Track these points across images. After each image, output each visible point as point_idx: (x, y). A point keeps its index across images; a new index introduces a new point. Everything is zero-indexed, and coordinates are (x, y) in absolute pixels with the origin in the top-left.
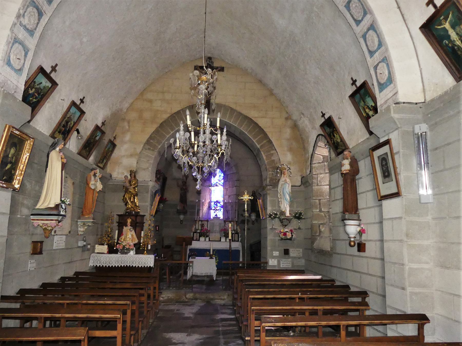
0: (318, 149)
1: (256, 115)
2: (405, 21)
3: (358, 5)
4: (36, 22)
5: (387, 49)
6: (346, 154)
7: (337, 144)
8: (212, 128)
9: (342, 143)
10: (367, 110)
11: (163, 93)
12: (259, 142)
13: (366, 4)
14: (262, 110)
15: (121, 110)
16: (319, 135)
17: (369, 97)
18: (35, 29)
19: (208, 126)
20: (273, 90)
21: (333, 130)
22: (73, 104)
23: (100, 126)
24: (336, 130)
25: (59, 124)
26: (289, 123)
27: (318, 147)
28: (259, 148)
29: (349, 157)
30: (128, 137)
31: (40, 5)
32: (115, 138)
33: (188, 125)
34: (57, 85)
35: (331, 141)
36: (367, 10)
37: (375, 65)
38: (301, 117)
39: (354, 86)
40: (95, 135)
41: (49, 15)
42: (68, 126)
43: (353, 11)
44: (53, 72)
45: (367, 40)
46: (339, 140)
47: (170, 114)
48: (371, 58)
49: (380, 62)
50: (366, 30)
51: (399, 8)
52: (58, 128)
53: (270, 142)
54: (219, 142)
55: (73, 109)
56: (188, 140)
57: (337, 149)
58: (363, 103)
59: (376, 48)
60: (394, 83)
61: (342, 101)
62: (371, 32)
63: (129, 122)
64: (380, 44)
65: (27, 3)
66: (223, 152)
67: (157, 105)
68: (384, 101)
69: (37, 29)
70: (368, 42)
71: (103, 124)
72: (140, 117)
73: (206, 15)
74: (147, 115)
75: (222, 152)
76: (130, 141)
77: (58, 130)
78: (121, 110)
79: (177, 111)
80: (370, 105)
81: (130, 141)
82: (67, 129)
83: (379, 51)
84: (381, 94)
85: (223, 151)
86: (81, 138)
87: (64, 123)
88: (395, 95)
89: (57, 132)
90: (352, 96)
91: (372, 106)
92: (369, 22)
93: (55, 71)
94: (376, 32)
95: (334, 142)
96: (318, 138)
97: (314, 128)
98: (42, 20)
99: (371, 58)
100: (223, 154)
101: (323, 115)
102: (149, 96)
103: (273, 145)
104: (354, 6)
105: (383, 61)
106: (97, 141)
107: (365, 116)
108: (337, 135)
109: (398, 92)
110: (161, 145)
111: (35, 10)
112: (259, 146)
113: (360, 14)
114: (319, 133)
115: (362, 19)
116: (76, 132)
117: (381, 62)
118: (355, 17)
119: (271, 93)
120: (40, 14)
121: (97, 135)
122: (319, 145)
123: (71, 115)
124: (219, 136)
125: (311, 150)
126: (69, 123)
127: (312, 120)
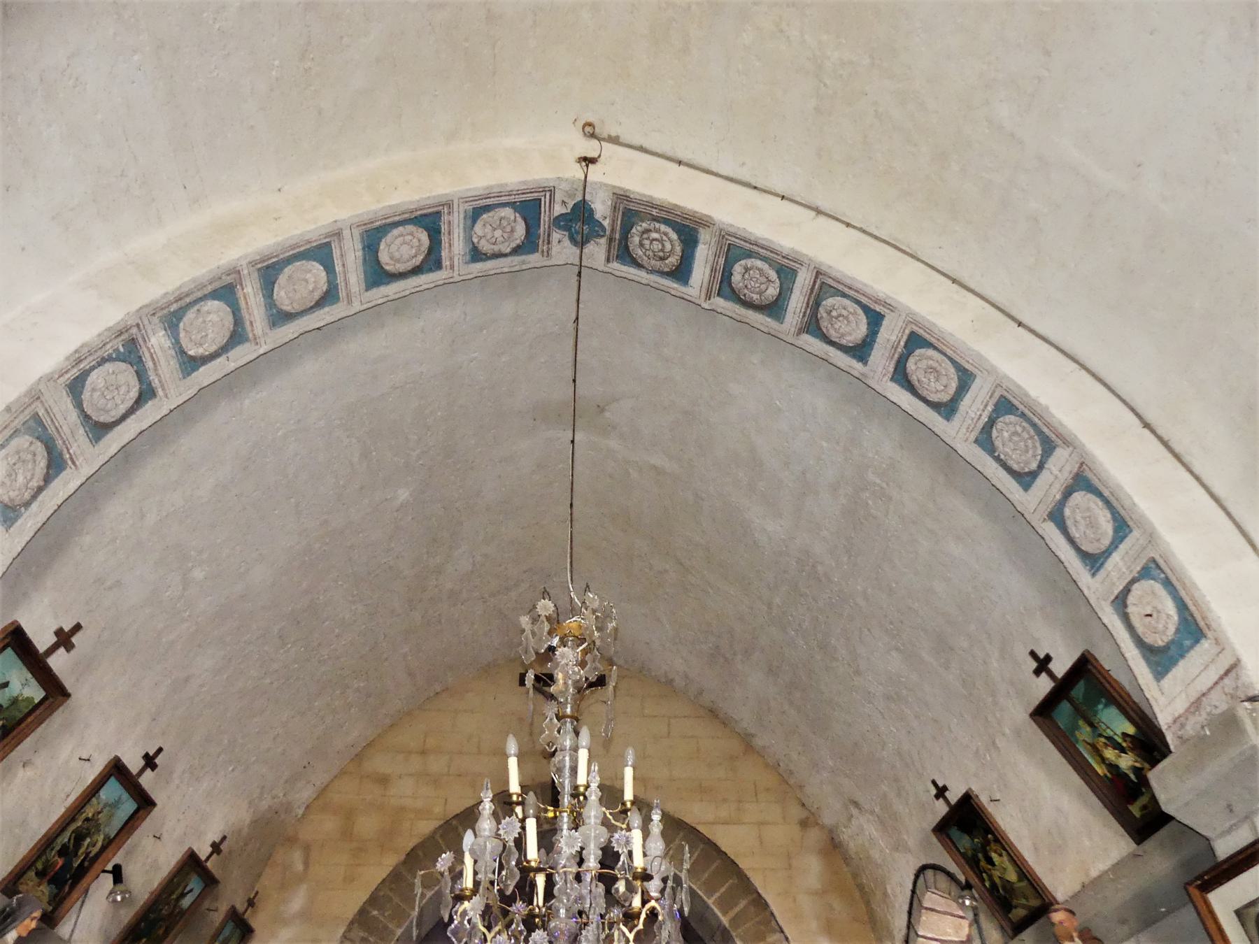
0: (925, 917)
1: (710, 817)
2: (1177, 456)
3: (1019, 429)
4: (35, 484)
5: (1151, 535)
6: (1061, 923)
7: (1004, 888)
8: (607, 809)
9: (1024, 884)
10: (1110, 754)
11: (423, 753)
12: (725, 907)
13: (1047, 425)
14: (725, 800)
15: (288, 808)
16: (923, 869)
17: (1106, 706)
18: (27, 504)
19: (594, 795)
20: (753, 736)
21: (985, 838)
22: (117, 769)
23: (203, 858)
24: (997, 840)
25: (47, 842)
26: (814, 835)
27: (923, 911)
28: (727, 925)
29: (1075, 934)
30: (297, 903)
31: (62, 438)
32: (251, 903)
33: (510, 795)
34: (65, 694)
35: (982, 881)
36: (1053, 437)
37: (1116, 592)
38: (852, 816)
39: (1044, 675)
40: (179, 891)
41: (86, 471)
42: (82, 850)
43: (1004, 449)
44: (62, 650)
45: (1069, 523)
46: (1012, 876)
47: (440, 819)
48: (1093, 575)
49: (1133, 581)
50: (1058, 497)
51: (1147, 425)
52: (39, 857)
53: (760, 903)
54: (639, 862)
55: (112, 790)
56: (514, 849)
57: (1009, 911)
58: (1088, 729)
59: (1106, 542)
60: (1210, 634)
61: (994, 743)
62: (1079, 497)
63: (307, 849)
64: (1122, 527)
65: (17, 421)
66: (654, 908)
67: (405, 791)
68: (1186, 705)
69: (34, 506)
70: (1074, 532)
71: (216, 847)
72: (347, 833)
73: (575, 445)
74: (368, 825)
75: (648, 906)
76: (306, 915)
77: (40, 866)
78: (288, 808)
79: (462, 809)
80: (1119, 732)
81: (306, 915)
82: (76, 865)
83: (1121, 546)
84: (1167, 681)
85: (653, 903)
86: (123, 899)
87: (65, 838)
88: (1233, 674)
89: (32, 874)
90: (1043, 712)
91: (1125, 735)
92: (1068, 468)
93: (69, 646)
94: (1100, 495)
95: (993, 884)
96: (921, 880)
97: (899, 846)
98: (56, 484)
99: (1093, 575)
100: (653, 914)
101: (941, 792)
102: (379, 763)
103: (772, 914)
104: (1006, 434)
105: (1145, 573)
106: (183, 913)
107: (1105, 775)
108: (1001, 855)
109: (1242, 663)
110: (404, 927)
111: (39, 448)
112: (725, 921)
113: (1031, 452)
114: (925, 863)
115: (1041, 466)
116: (109, 879)
117: (1139, 580)
118: (1015, 467)
119: (748, 744)
120: (56, 464)
121: (188, 889)
122: (926, 904)
123: (99, 813)
124: (637, 835)
125: (900, 922)
126: (88, 840)
127: (890, 821)
